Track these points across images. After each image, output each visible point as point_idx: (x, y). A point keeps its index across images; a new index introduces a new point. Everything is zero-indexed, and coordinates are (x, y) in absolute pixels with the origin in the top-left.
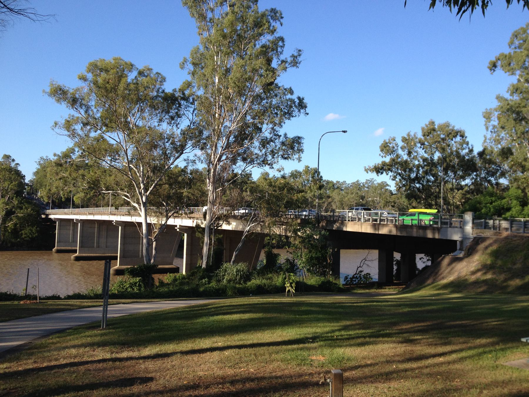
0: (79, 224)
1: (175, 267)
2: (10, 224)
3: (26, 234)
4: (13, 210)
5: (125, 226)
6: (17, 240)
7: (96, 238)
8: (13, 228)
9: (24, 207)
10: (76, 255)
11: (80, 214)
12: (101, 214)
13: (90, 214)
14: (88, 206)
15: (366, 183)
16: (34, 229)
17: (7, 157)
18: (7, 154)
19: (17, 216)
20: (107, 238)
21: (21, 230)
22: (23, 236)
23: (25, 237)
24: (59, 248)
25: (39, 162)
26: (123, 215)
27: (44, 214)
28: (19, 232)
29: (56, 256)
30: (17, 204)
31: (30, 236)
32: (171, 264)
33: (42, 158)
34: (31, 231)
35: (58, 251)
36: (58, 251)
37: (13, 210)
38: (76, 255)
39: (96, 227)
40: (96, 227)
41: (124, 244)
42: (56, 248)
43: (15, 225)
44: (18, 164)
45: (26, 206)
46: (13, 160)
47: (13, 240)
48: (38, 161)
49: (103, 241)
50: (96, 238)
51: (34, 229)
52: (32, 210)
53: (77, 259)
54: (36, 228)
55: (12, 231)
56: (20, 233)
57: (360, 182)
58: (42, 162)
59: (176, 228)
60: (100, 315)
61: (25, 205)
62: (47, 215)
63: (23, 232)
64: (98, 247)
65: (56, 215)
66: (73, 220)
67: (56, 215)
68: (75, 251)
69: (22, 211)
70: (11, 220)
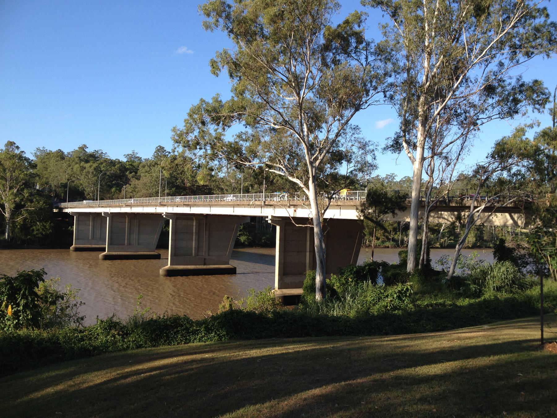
0: (108, 218)
1: (231, 267)
2: (19, 219)
3: (38, 230)
4: (22, 203)
5: (176, 220)
6: (27, 237)
7: (126, 234)
8: (22, 223)
9: (34, 200)
10: (105, 253)
11: (110, 207)
12: (143, 206)
13: (127, 206)
14: (112, 199)
15: (386, 178)
16: (47, 225)
17: (11, 144)
18: (12, 141)
19: (27, 210)
20: (139, 234)
21: (32, 226)
22: (35, 233)
23: (37, 234)
24: (78, 246)
25: (35, 153)
26: (177, 206)
27: (56, 208)
28: (30, 228)
29: (74, 254)
30: (27, 197)
31: (44, 233)
32: (227, 263)
33: (38, 149)
34: (45, 226)
35: (77, 250)
36: (77, 250)
37: (22, 203)
38: (105, 253)
39: (127, 221)
40: (127, 221)
41: (175, 240)
42: (74, 246)
43: (25, 219)
44: (22, 152)
45: (37, 198)
46: (18, 148)
47: (23, 237)
48: (33, 152)
49: (134, 237)
50: (126, 234)
51: (47, 225)
52: (44, 203)
53: (106, 258)
54: (50, 223)
55: (21, 227)
56: (32, 229)
57: (380, 177)
58: (38, 153)
59: (267, 219)
60: (545, 329)
61: (35, 198)
62: (61, 209)
63: (34, 227)
64: (129, 244)
65: (71, 208)
66: (100, 213)
67: (71, 208)
68: (103, 250)
69: (33, 204)
70: (21, 214)
